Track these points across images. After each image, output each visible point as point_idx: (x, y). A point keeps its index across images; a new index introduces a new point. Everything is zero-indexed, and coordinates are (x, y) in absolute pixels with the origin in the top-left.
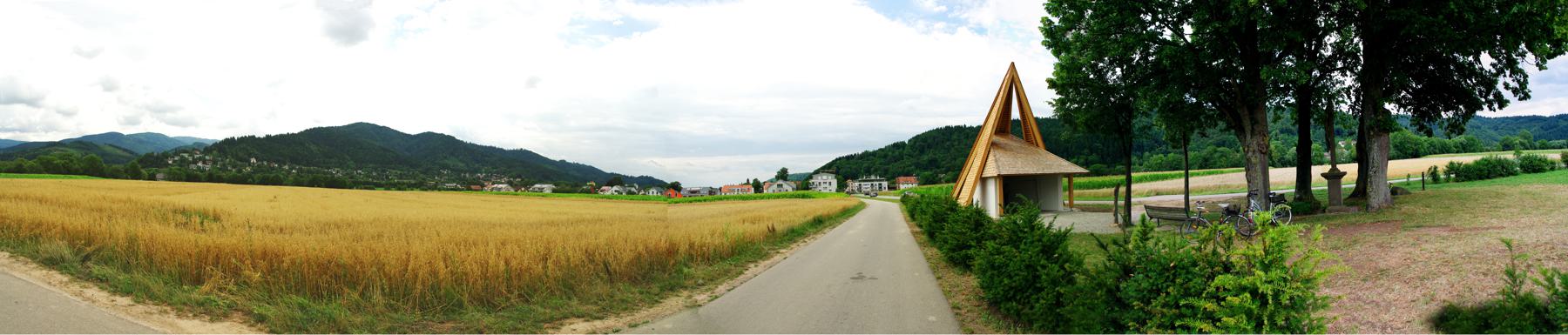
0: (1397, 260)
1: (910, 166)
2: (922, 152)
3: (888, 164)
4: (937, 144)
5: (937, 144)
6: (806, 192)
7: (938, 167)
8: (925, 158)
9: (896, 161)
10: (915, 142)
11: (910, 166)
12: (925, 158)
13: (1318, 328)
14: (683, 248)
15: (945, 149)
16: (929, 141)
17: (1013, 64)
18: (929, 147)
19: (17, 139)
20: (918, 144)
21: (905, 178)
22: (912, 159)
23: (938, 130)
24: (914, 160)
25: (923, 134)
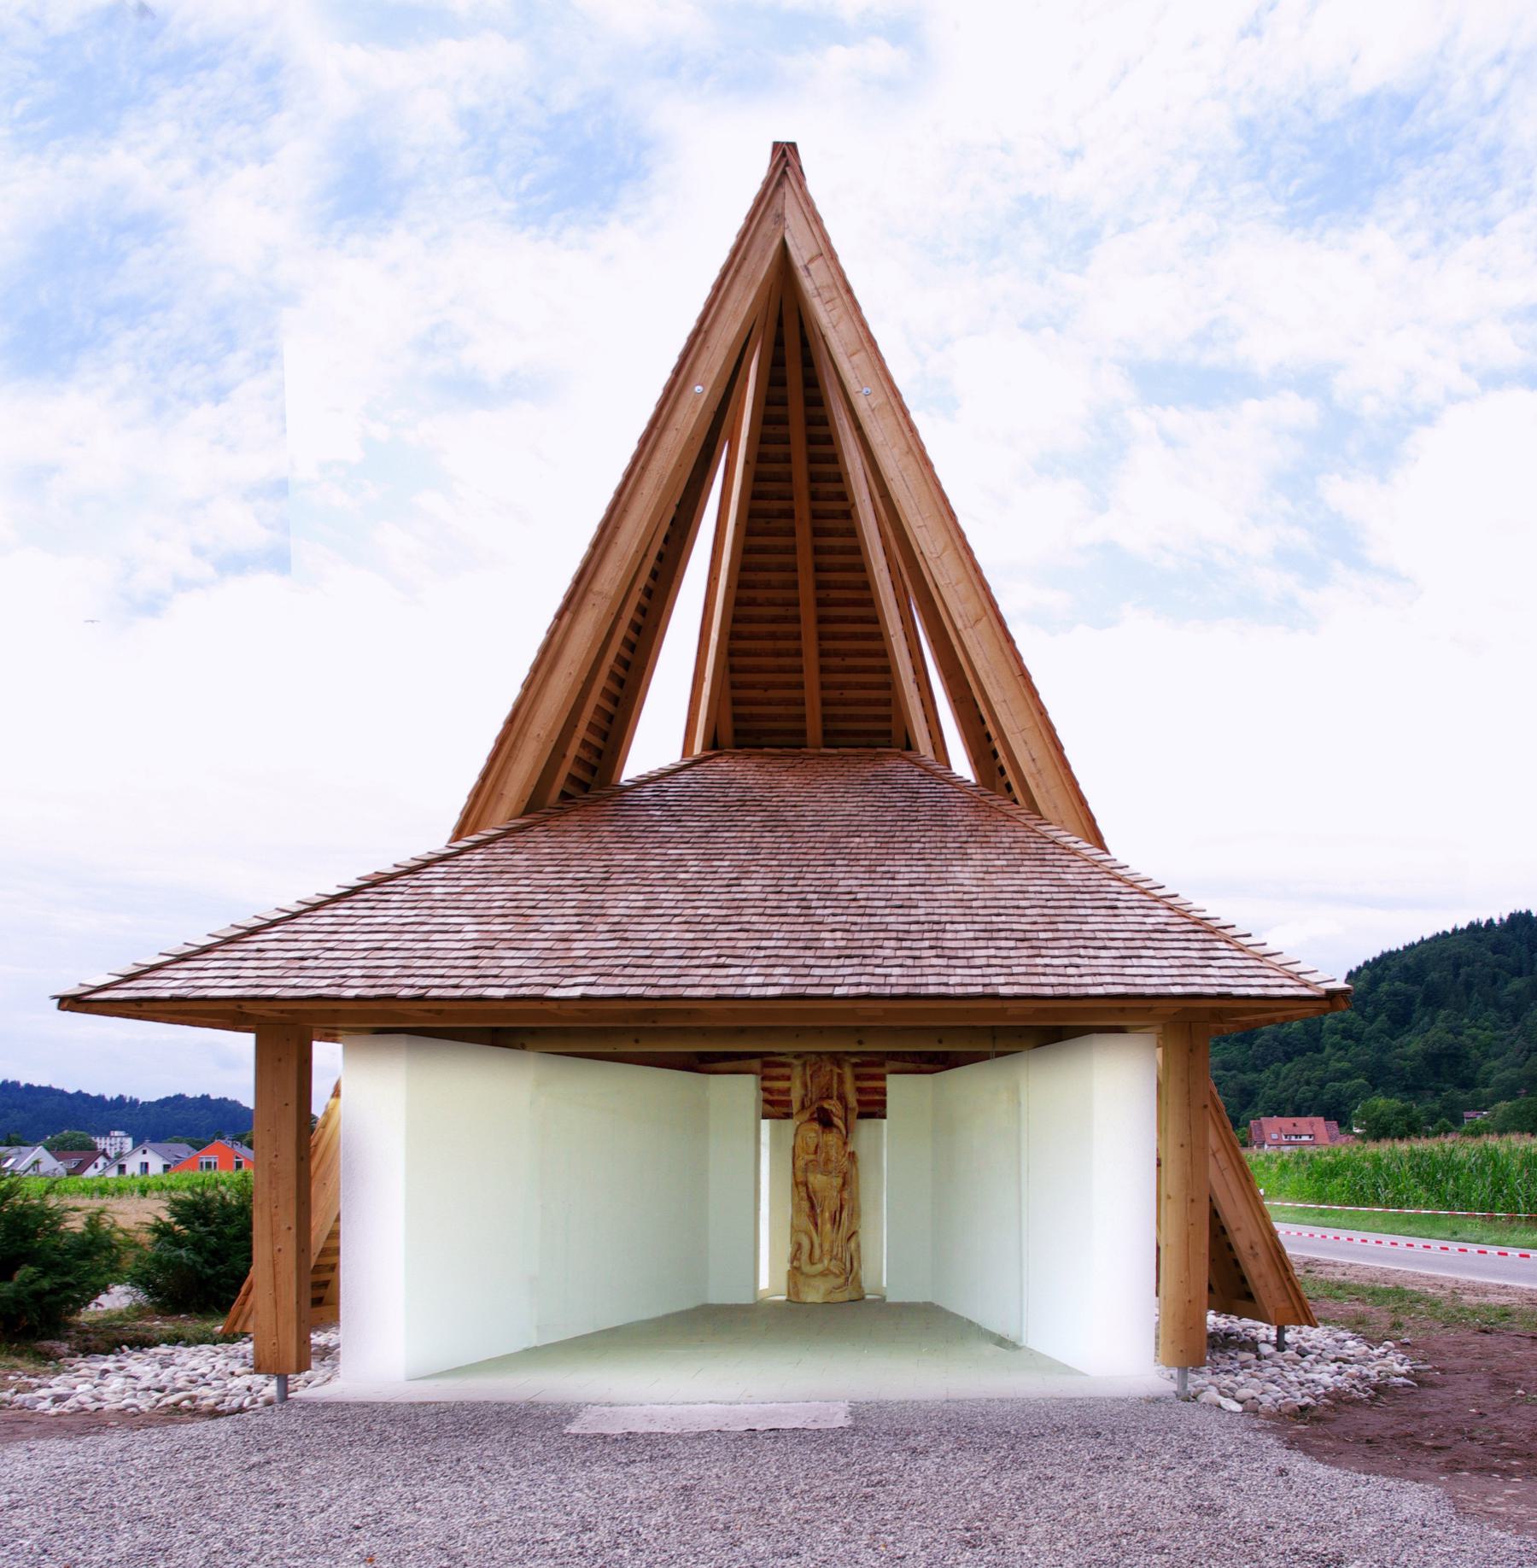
0: (340, 1560)
1: (1346, 1075)
2: (1401, 1020)
3: (1257, 1069)
4: (1469, 986)
5: (1469, 986)
6: (1230, 1126)
7: (1466, 1084)
8: (1414, 1044)
9: (1288, 1058)
10: (1374, 982)
11: (1346, 1075)
12: (1414, 1044)
13: (1256, 1412)
14: (1496, 1135)
15: (1499, 1007)
16: (1434, 976)
17: (785, 157)
18: (1433, 1000)
19: (776, 250)
20: (1384, 987)
21: (1286, 1122)
22: (1354, 1050)
23: (1476, 932)
24: (1367, 1054)
25: (1410, 948)
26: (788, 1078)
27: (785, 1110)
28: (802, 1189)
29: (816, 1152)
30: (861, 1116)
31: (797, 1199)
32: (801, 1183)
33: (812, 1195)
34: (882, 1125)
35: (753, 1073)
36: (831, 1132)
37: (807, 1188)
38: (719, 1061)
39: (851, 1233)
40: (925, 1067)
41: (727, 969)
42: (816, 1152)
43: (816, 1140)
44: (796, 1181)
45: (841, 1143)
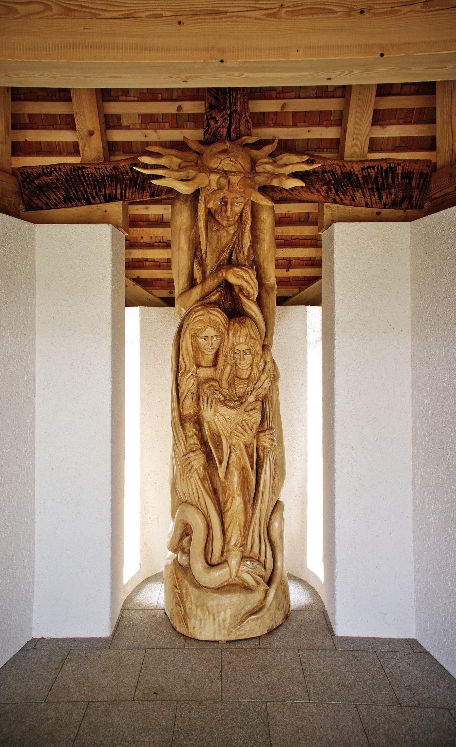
26: (168, 245)
27: (164, 293)
28: (191, 430)
29: (215, 364)
30: (281, 301)
31: (182, 448)
32: (190, 418)
33: (219, 489)
34: (304, 317)
35: (108, 223)
36: (242, 324)
37: (200, 430)
38: (56, 206)
39: (274, 502)
40: (386, 212)
41: (255, 545)
42: (215, 364)
43: (216, 342)
44: (180, 414)
45: (259, 348)
